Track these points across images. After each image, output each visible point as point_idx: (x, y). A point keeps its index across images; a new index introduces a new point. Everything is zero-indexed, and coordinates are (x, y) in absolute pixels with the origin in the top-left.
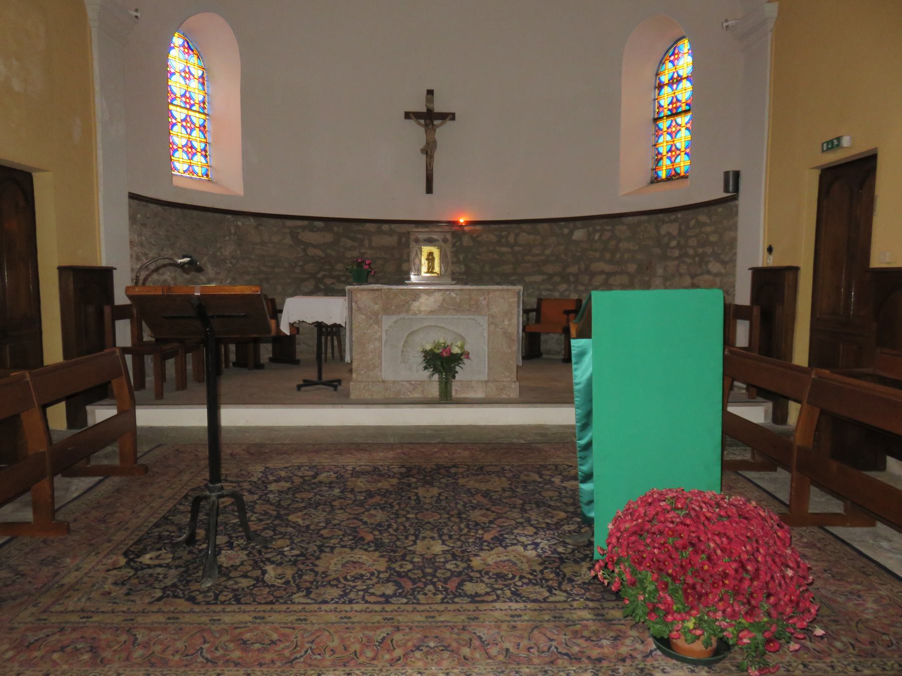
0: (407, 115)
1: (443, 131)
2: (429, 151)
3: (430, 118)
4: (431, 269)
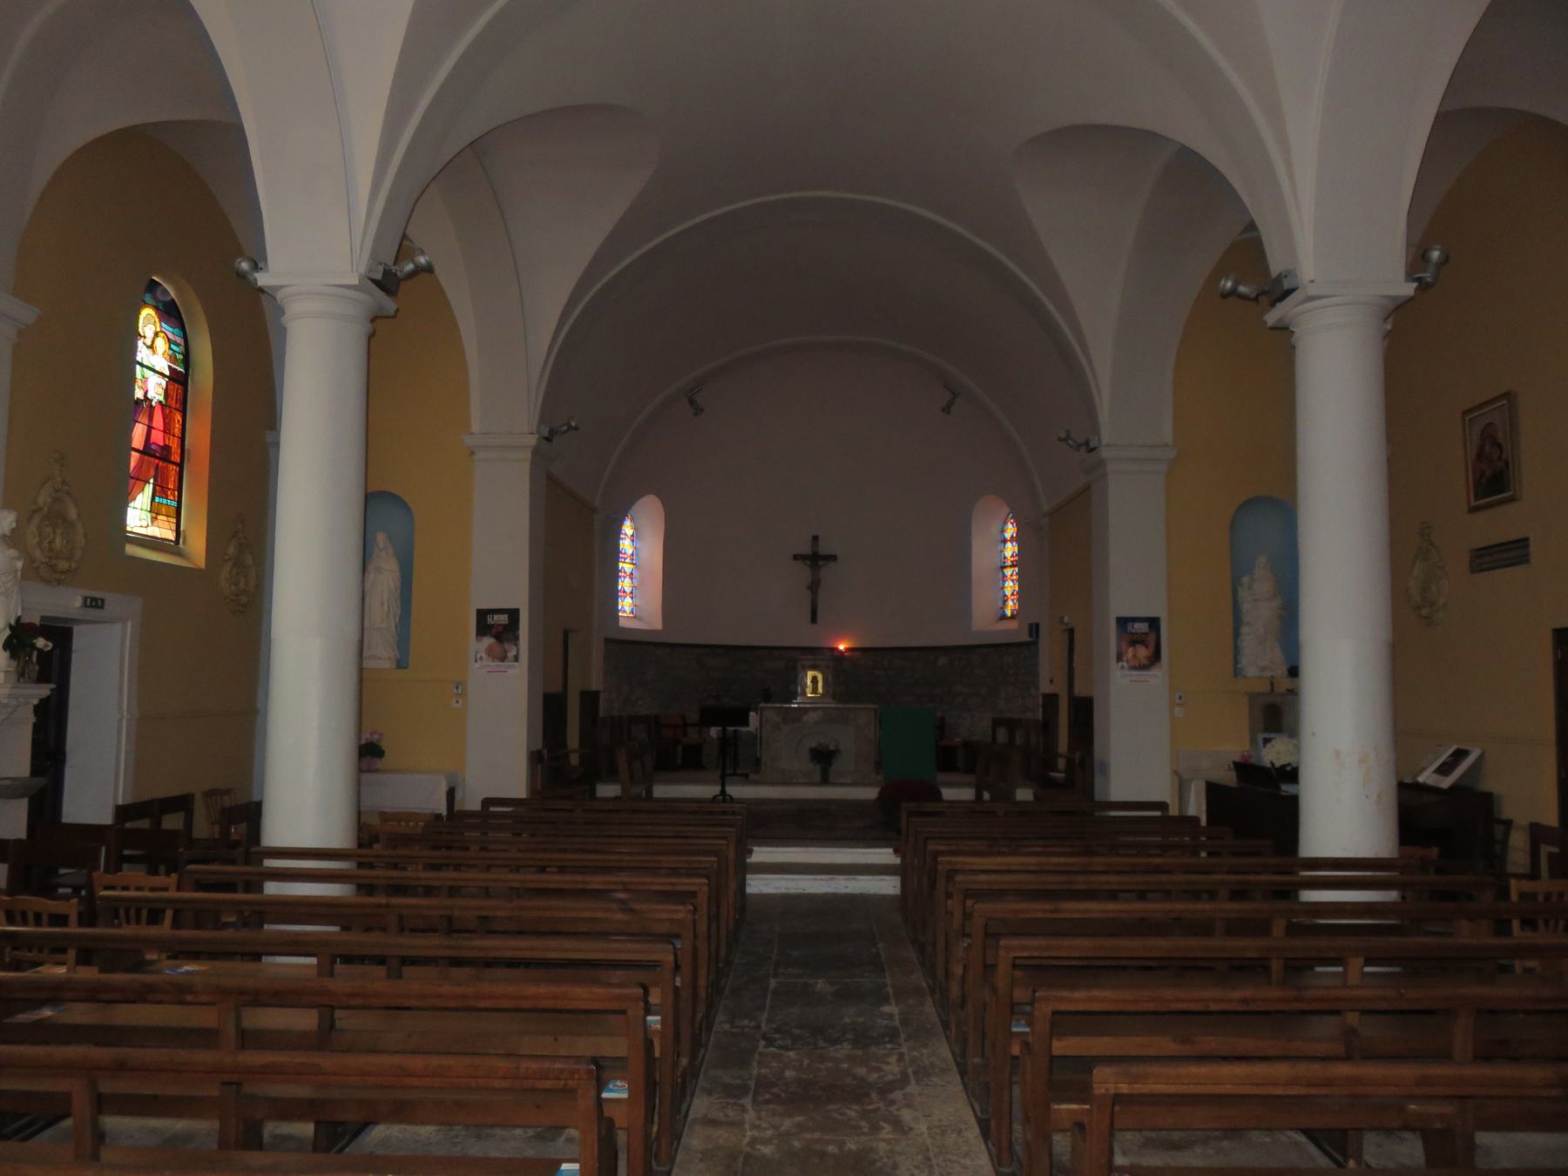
0: (796, 557)
1: (828, 573)
2: (814, 587)
3: (815, 559)
4: (815, 690)
